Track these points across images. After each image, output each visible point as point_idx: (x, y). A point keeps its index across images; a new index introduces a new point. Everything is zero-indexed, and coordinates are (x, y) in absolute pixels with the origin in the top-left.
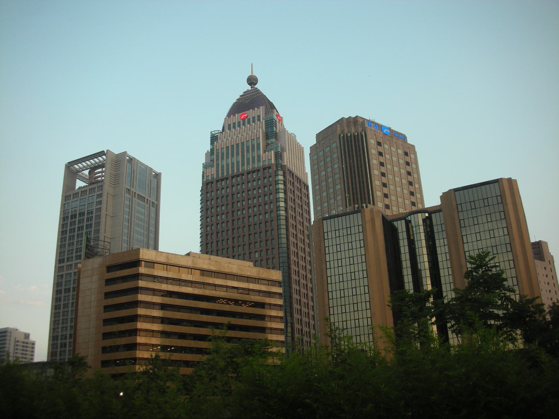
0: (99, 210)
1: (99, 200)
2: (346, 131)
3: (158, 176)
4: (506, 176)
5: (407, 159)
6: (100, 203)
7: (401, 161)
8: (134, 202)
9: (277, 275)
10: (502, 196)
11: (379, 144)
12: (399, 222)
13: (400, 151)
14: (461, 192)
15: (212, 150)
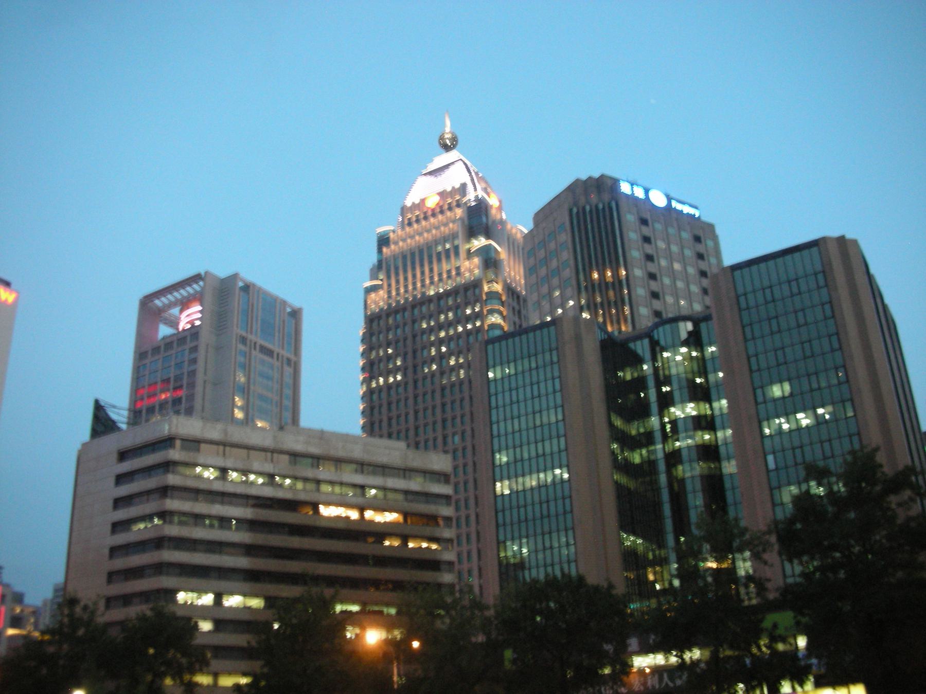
0: (192, 374)
1: (193, 356)
2: (582, 201)
3: (296, 314)
4: (835, 233)
5: (700, 248)
6: (194, 361)
7: (688, 253)
8: (253, 357)
9: (440, 462)
10: (826, 271)
11: (644, 222)
12: (639, 343)
13: (685, 235)
14: (746, 271)
15: (380, 262)
